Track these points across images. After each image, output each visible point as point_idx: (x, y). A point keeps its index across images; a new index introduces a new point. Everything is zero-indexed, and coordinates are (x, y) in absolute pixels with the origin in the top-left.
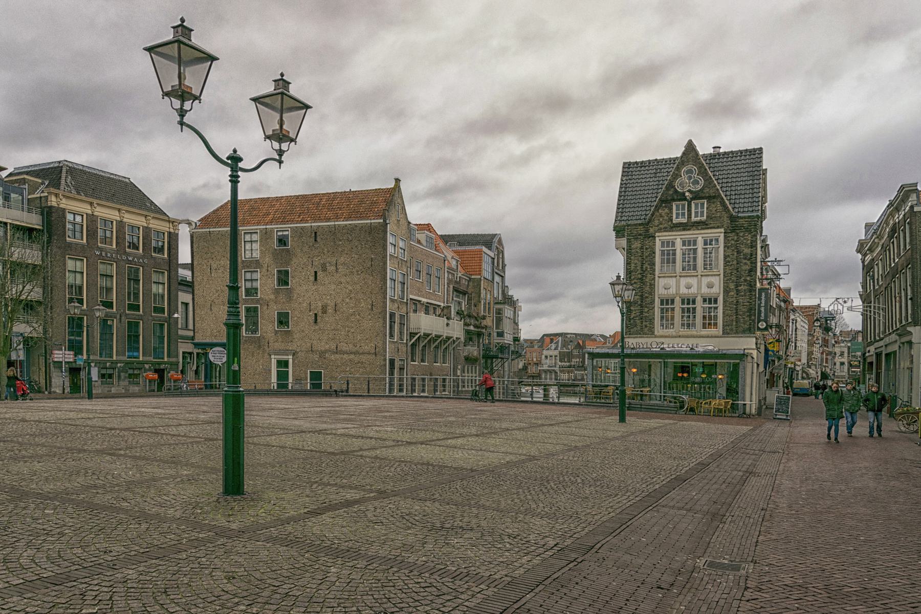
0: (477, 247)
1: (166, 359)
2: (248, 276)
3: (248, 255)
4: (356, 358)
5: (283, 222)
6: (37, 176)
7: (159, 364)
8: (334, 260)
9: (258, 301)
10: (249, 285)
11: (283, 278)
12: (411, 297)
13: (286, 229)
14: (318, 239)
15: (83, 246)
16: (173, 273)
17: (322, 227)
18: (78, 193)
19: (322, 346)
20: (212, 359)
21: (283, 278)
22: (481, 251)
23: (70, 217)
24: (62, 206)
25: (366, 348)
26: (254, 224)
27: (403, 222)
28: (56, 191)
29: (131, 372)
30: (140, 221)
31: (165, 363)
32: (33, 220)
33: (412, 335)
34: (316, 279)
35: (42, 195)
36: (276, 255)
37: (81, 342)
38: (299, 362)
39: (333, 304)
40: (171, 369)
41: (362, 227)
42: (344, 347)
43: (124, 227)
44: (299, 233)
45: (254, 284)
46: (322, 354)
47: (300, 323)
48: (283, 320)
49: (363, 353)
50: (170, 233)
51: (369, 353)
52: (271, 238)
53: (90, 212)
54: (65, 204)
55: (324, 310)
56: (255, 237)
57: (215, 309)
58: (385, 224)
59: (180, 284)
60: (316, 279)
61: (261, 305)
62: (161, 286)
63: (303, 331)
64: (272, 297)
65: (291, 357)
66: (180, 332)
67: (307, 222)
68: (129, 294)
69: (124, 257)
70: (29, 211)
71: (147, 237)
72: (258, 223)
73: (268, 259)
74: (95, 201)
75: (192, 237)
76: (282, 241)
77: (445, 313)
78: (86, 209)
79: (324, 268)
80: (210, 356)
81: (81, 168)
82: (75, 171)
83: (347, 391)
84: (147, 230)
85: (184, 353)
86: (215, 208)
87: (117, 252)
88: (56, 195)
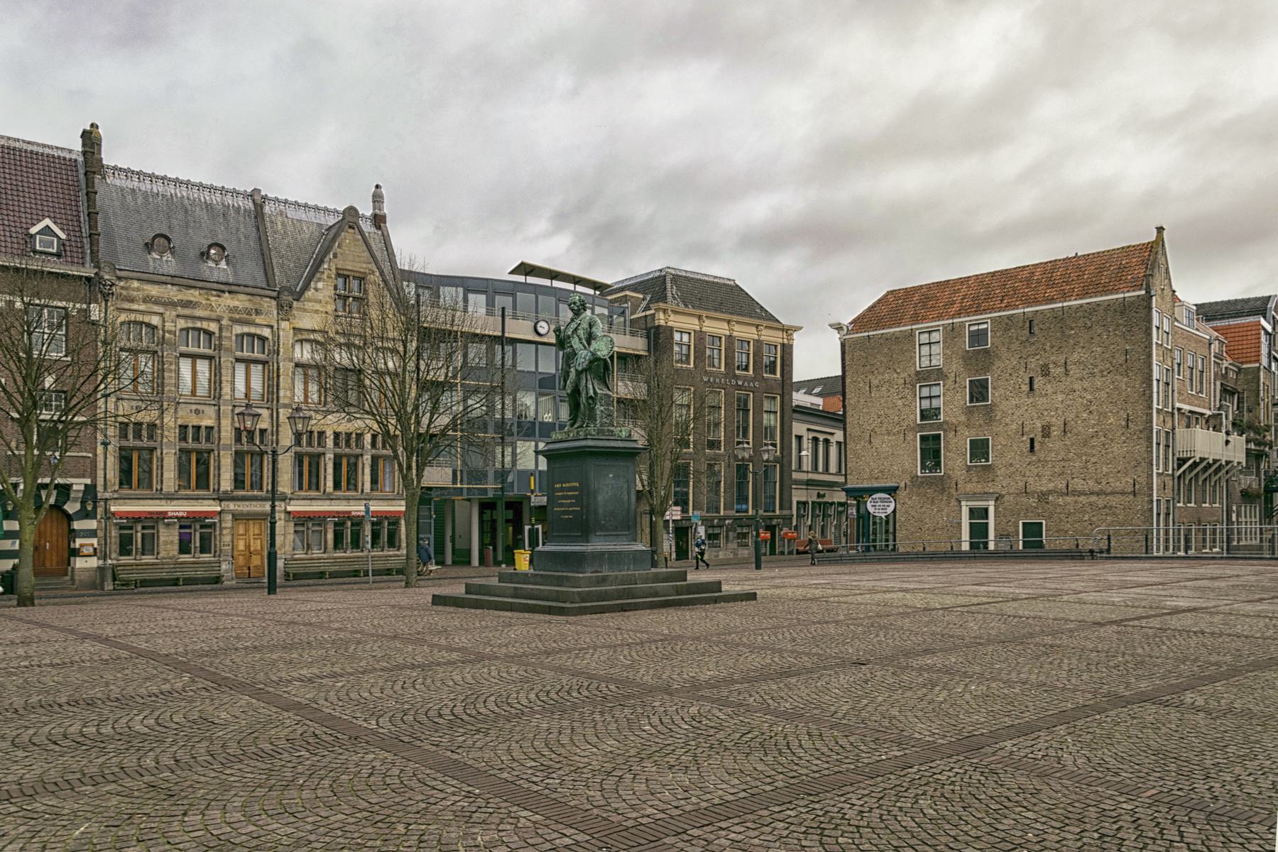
0: (1251, 319)
1: (778, 512)
2: (925, 392)
3: (925, 363)
4: (1101, 501)
5: (977, 312)
6: (635, 290)
7: (771, 518)
8: (1062, 359)
9: (940, 426)
10: (926, 404)
11: (979, 391)
12: (1178, 405)
13: (985, 320)
14: (1036, 329)
15: (689, 370)
16: (786, 398)
17: (1042, 312)
18: (686, 306)
19: (1045, 485)
20: (871, 510)
21: (979, 391)
22: (1259, 323)
23: (677, 336)
24: (670, 324)
25: (1118, 486)
26: (933, 319)
27: (1167, 291)
28: (662, 305)
29: (739, 530)
30: (744, 332)
31: (778, 517)
32: (636, 344)
33: (1182, 461)
34: (1031, 389)
35: (648, 313)
36: (968, 359)
37: (687, 494)
38: (1005, 509)
39: (1061, 423)
40: (784, 525)
41: (1109, 305)
42: (1078, 484)
43: (733, 344)
44: (1005, 325)
45: (935, 403)
46: (1043, 496)
47: (1006, 451)
48: (979, 449)
49: (1112, 493)
50: (783, 345)
51: (1123, 493)
52: (962, 336)
53: (697, 328)
54: (675, 321)
55: (1046, 431)
56: (936, 337)
57: (876, 442)
58: (1149, 297)
59: (794, 411)
60: (1031, 389)
61: (945, 431)
62: (772, 416)
63: (1011, 465)
64: (963, 418)
65: (992, 503)
66: (795, 476)
67: (1016, 307)
68: (738, 428)
69: (733, 382)
70: (633, 334)
71: (758, 354)
72: (940, 317)
73: (956, 366)
74: (704, 313)
75: (843, 345)
76: (979, 337)
77: (1213, 423)
78: (693, 324)
79: (1045, 371)
80: (869, 505)
81: (684, 274)
82: (680, 280)
83: (1108, 551)
84: (758, 343)
85: (798, 503)
86: (870, 304)
87: (726, 375)
88: (665, 311)
